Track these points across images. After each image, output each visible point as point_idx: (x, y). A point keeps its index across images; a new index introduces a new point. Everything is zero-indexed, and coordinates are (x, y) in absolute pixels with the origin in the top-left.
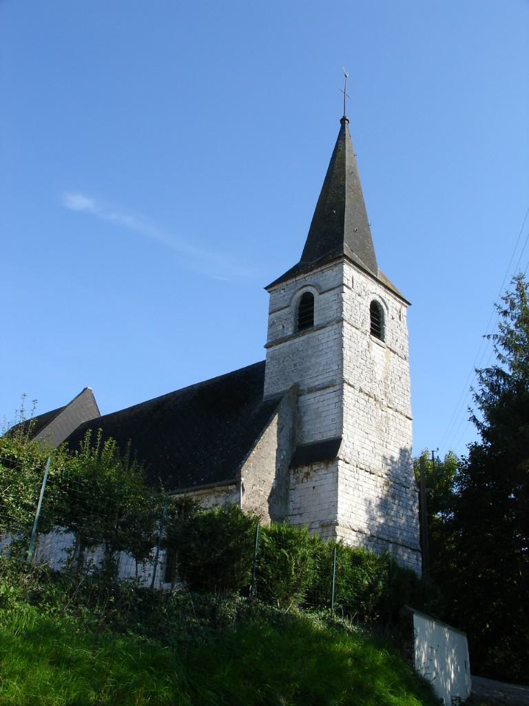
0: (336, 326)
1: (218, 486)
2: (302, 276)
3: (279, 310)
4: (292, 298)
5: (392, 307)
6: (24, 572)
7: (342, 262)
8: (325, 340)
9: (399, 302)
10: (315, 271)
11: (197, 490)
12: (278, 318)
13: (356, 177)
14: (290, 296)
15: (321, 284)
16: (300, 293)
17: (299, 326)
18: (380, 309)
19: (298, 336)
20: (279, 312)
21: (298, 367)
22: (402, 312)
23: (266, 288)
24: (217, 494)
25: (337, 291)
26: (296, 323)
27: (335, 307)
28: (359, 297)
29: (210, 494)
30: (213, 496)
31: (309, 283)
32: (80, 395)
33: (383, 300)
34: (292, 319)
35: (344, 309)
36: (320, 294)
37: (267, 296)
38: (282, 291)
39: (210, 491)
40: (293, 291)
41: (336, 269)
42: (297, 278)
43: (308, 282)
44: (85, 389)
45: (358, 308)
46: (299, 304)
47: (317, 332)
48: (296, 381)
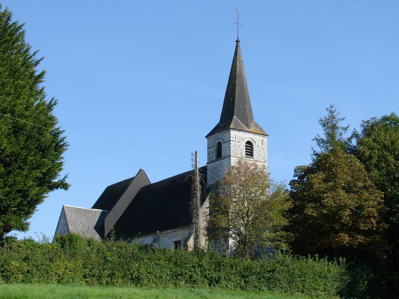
0: (228, 158)
1: (188, 226)
2: (217, 134)
3: (210, 148)
4: (214, 143)
5: (257, 140)
6: (257, 272)
7: (230, 130)
8: (226, 164)
9: (262, 136)
10: (221, 132)
11: (182, 227)
12: (211, 151)
13: (242, 77)
14: (214, 142)
15: (224, 139)
16: (217, 141)
17: (218, 156)
18: (251, 143)
19: (217, 161)
20: (210, 149)
21: (218, 174)
22: (264, 140)
23: (196, 153)
24: (188, 229)
25: (229, 142)
26: (216, 154)
27: (228, 150)
28: (239, 143)
29: (186, 229)
30: (187, 230)
31: (220, 138)
32: (138, 173)
33: (252, 139)
34: (215, 153)
35: (231, 151)
36: (224, 143)
37: (206, 140)
38: (211, 139)
39: (186, 228)
40: (215, 140)
41: (228, 133)
42: (216, 135)
43: (220, 136)
44: (140, 170)
45: (238, 148)
46: (217, 145)
47: (223, 160)
48: (217, 180)
